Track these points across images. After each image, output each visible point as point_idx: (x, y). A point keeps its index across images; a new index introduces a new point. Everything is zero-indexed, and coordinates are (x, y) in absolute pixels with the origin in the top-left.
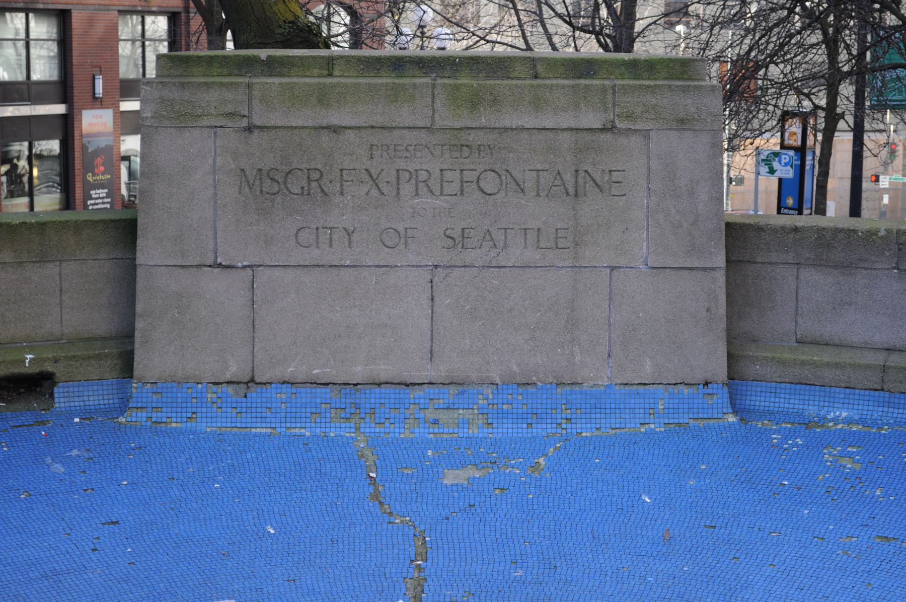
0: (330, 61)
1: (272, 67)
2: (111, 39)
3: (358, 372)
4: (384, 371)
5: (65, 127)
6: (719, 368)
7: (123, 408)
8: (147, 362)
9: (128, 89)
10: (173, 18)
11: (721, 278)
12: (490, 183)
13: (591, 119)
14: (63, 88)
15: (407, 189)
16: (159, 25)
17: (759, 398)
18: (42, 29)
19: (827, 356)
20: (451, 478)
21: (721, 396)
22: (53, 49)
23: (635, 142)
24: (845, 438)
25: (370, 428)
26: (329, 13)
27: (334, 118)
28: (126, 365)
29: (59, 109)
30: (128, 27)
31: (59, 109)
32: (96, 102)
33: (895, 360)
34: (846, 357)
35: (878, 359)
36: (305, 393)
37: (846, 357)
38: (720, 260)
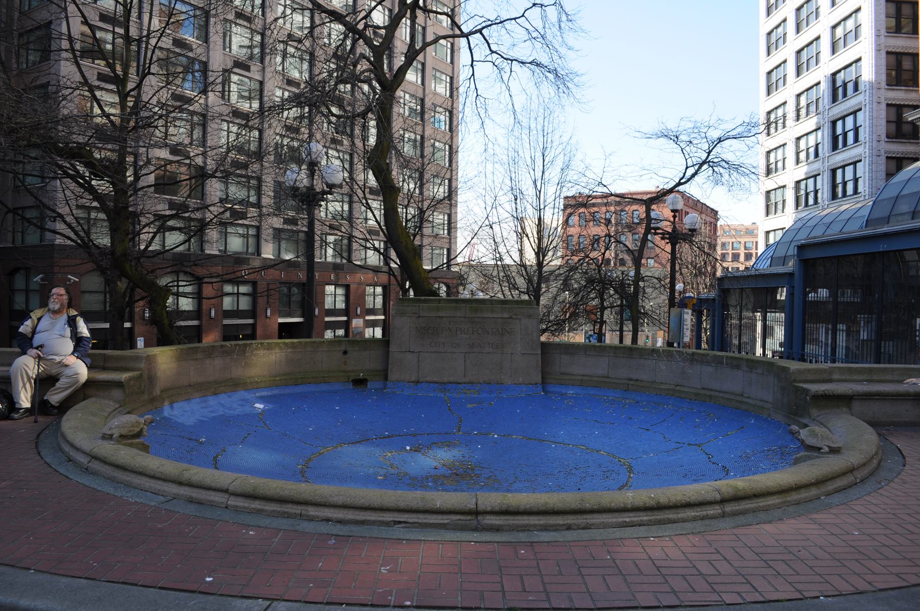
0: (439, 301)
1: (425, 301)
2: (363, 295)
3: (446, 380)
4: (452, 379)
5: (346, 325)
6: (539, 379)
7: (385, 388)
8: (392, 376)
9: (372, 312)
10: (385, 288)
11: (540, 356)
12: (480, 331)
13: (506, 315)
14: (346, 312)
15: (459, 333)
16: (379, 290)
17: (551, 388)
18: (340, 291)
19: (568, 377)
20: (469, 406)
21: (540, 387)
22: (343, 298)
23: (518, 321)
24: (570, 398)
25: (448, 394)
26: (423, 164)
27: (440, 314)
28: (386, 378)
29: (345, 318)
30: (370, 290)
31: (345, 318)
32: (357, 316)
33: (585, 378)
34: (573, 377)
35: (580, 378)
36: (432, 385)
37: (573, 377)
38: (540, 352)
